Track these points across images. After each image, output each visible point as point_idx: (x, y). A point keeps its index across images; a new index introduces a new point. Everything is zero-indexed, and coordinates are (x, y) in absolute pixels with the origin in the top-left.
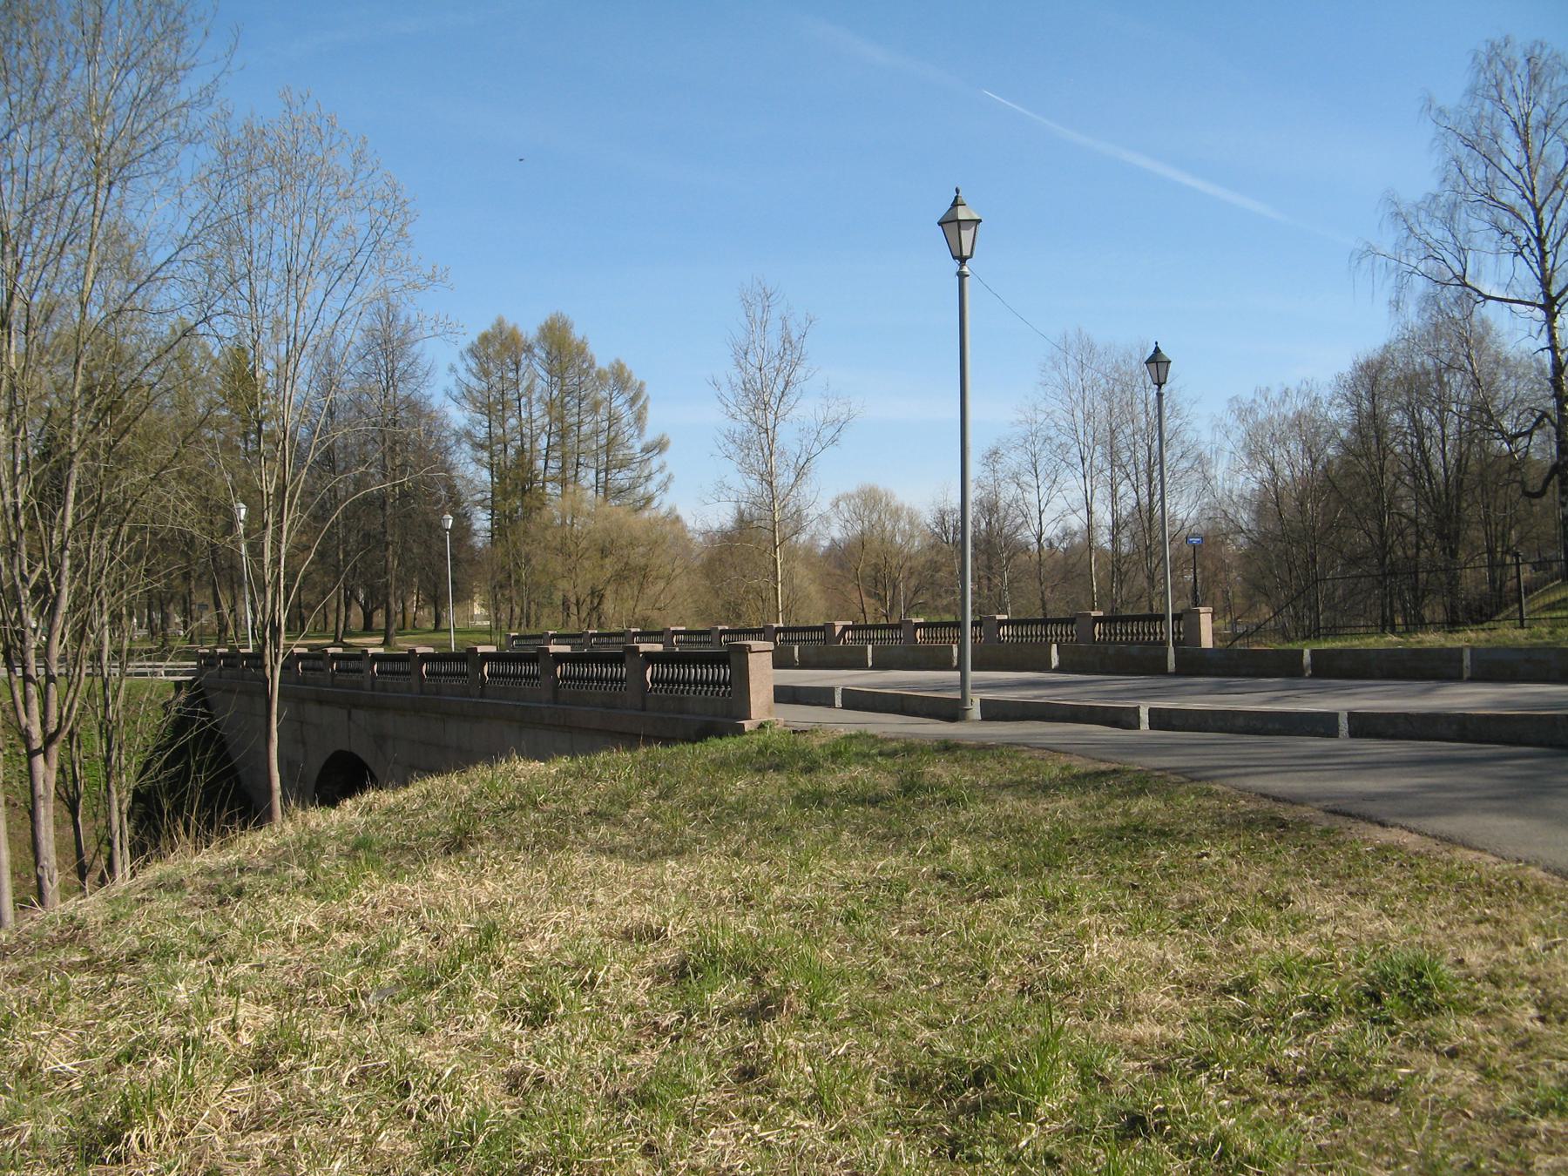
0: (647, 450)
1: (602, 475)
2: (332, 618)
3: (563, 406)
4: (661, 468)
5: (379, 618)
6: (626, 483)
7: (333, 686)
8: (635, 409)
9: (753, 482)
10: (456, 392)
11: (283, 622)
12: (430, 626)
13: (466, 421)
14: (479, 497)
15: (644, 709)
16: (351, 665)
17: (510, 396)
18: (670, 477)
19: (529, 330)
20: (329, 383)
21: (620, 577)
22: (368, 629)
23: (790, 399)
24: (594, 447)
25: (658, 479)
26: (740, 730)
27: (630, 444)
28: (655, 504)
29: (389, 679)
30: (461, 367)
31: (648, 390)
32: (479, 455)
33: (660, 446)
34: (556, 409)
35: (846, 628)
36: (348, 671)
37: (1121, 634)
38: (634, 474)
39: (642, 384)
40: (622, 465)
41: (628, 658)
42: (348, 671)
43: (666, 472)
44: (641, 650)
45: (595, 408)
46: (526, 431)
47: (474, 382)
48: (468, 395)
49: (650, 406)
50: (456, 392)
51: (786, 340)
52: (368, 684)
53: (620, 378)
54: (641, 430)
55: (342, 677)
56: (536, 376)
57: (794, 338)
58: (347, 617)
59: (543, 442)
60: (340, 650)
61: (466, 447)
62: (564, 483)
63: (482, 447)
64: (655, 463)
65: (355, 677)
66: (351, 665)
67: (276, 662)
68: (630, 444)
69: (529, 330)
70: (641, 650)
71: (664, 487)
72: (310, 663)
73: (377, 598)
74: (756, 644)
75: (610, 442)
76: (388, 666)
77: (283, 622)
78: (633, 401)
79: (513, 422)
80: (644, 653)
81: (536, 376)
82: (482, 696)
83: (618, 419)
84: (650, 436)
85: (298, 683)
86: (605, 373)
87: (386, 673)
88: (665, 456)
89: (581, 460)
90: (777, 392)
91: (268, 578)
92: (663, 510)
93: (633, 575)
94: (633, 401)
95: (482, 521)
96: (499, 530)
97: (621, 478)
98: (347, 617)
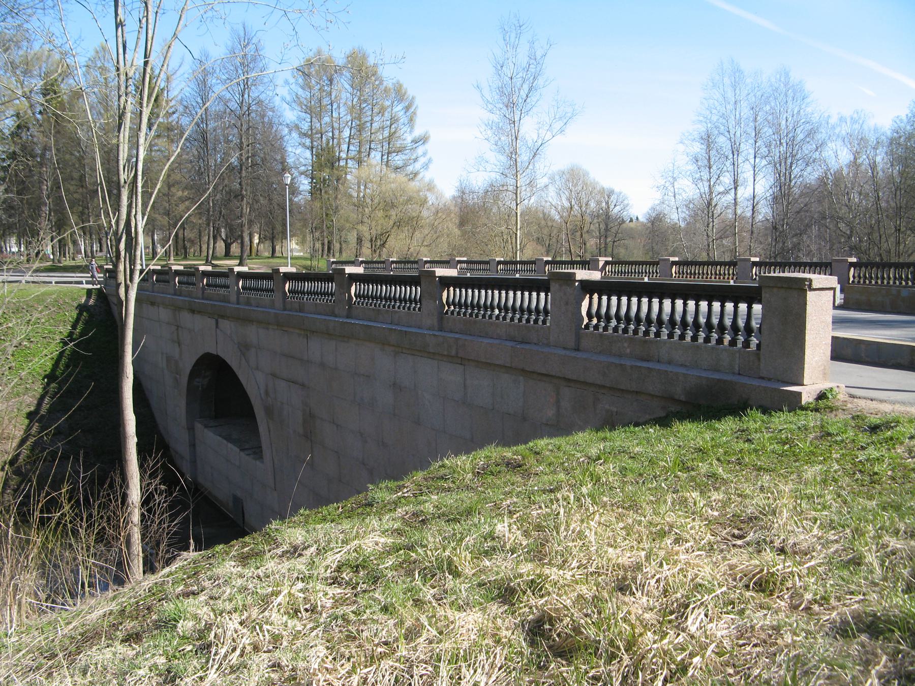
0: (415, 141)
1: (385, 157)
2: (204, 247)
3: (361, 109)
4: (425, 154)
5: (235, 248)
6: (400, 163)
7: (203, 299)
8: (408, 114)
9: (503, 158)
10: (288, 98)
11: (140, 230)
12: (267, 254)
13: (295, 118)
14: (303, 168)
15: (577, 349)
16: (219, 281)
17: (326, 101)
18: (430, 160)
19: (339, 58)
20: (203, 88)
21: (398, 224)
22: (227, 255)
23: (532, 99)
24: (381, 138)
25: (422, 160)
26: (794, 403)
27: (404, 137)
28: (420, 176)
29: (253, 295)
30: (292, 80)
31: (417, 102)
32: (303, 141)
33: (424, 139)
34: (357, 113)
35: (607, 263)
36: (216, 286)
37: (877, 278)
38: (407, 157)
39: (413, 98)
40: (399, 151)
41: (554, 286)
42: (216, 286)
43: (428, 157)
44: (578, 277)
45: (382, 111)
46: (336, 125)
47: (300, 92)
48: (297, 100)
49: (419, 113)
50: (288, 98)
51: (532, 57)
52: (233, 298)
53: (399, 93)
54: (412, 127)
55: (210, 291)
56: (343, 87)
57: (539, 54)
58: (214, 248)
59: (346, 133)
60: (209, 268)
61: (295, 135)
62: (360, 162)
63: (305, 135)
64: (420, 150)
65: (222, 291)
66: (219, 281)
67: (131, 280)
68: (404, 137)
69: (339, 58)
70: (578, 277)
71: (426, 166)
72: (185, 279)
73: (235, 235)
74: (819, 279)
75: (391, 136)
76: (252, 283)
77: (140, 230)
78: (407, 108)
79: (327, 119)
80: (581, 281)
81: (343, 87)
82: (348, 317)
83: (397, 120)
84: (418, 132)
85: (175, 294)
86: (390, 89)
87: (250, 289)
88: (427, 146)
89: (372, 146)
90: (523, 94)
91: (123, 176)
92: (427, 179)
93: (409, 223)
94: (407, 108)
95: (305, 184)
96: (315, 191)
97: (397, 159)
98: (214, 248)
